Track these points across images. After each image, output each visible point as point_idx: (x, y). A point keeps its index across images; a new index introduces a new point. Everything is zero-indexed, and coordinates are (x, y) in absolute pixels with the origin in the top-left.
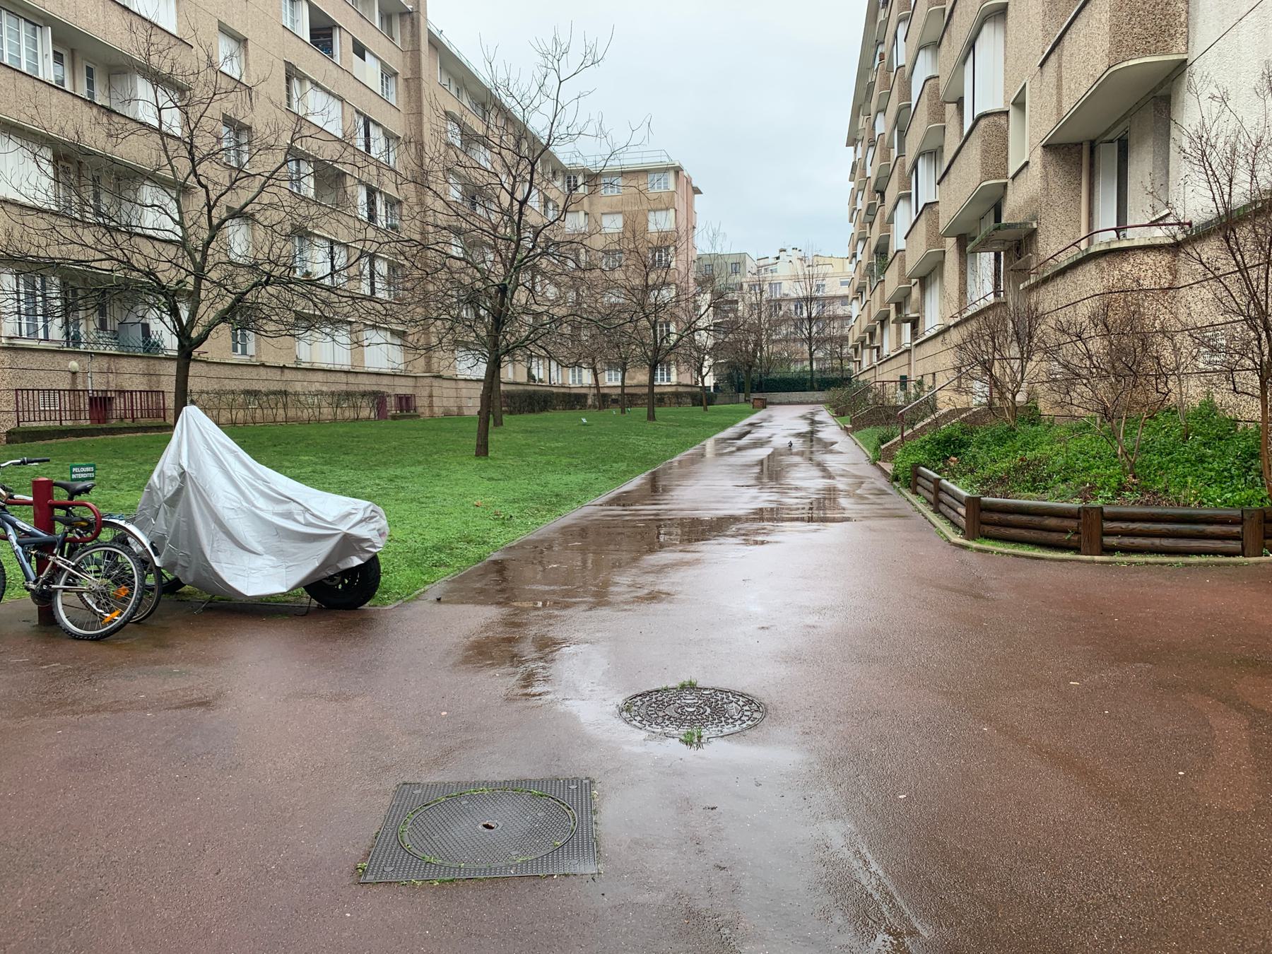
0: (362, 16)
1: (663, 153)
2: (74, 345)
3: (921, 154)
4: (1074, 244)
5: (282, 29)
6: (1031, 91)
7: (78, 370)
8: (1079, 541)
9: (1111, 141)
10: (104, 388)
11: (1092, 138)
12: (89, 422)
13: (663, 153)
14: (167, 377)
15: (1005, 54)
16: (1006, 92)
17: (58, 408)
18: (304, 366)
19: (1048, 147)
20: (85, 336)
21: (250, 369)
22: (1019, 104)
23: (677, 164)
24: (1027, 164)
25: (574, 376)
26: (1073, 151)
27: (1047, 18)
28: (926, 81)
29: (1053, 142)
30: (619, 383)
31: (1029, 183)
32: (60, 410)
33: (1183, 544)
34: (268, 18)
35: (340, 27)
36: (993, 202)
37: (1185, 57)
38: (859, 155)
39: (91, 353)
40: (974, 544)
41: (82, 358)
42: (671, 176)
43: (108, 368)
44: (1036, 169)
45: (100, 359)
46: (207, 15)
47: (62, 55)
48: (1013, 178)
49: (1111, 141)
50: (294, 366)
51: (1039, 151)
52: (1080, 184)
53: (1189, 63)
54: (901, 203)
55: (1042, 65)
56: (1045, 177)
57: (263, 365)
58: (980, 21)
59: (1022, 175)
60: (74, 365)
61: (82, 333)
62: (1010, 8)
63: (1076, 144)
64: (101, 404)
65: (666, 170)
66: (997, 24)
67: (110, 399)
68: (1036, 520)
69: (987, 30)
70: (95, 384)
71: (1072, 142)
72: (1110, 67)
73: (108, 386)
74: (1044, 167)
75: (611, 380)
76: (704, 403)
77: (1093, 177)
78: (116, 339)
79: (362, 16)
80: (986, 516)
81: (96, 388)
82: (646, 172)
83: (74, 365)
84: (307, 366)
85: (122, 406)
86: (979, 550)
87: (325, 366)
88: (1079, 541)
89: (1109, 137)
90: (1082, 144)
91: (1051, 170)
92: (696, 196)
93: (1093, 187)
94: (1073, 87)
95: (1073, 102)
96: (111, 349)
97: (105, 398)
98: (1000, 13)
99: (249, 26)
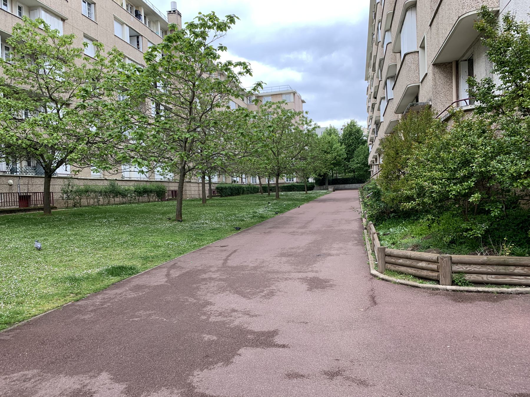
0: (152, 31)
1: (288, 86)
2: (11, 173)
3: (388, 78)
4: (445, 110)
5: (114, 36)
6: (427, 39)
7: (12, 184)
8: (438, 276)
9: (466, 60)
10: (26, 191)
11: (457, 59)
12: (18, 207)
13: (288, 86)
14: (58, 186)
15: (417, 25)
16: (418, 43)
17: (3, 201)
18: (125, 179)
19: (436, 65)
20: (19, 169)
21: (99, 181)
22: (422, 47)
23: (294, 91)
24: (426, 74)
25: (253, 180)
26: (448, 66)
27: (433, 3)
28: (387, 45)
29: (436, 62)
30: (275, 182)
31: (428, 84)
32: (4, 202)
33: (501, 279)
34: (108, 32)
35: (142, 36)
36: (415, 96)
37: (498, 9)
38: (369, 83)
39: (19, 176)
40: (382, 276)
41: (15, 178)
42: (292, 95)
43: (28, 183)
44: (430, 77)
45: (24, 179)
46: (78, 31)
47: (9, 48)
48: (422, 82)
49: (466, 60)
50: (121, 179)
51: (431, 67)
52: (452, 82)
53: (500, 12)
54: (382, 100)
55: (430, 25)
56: (434, 79)
57: (106, 179)
58: (405, 11)
59: (425, 80)
60: (11, 182)
61: (18, 168)
62: (418, 3)
63: (449, 63)
64: (25, 199)
65: (290, 93)
66: (412, 11)
67: (30, 196)
68: (414, 263)
69: (408, 14)
70: (24, 190)
71: (447, 61)
72: (459, 17)
73: (28, 191)
74: (434, 75)
75: (265, 181)
76: (306, 190)
77: (458, 78)
78: (35, 170)
79: (152, 31)
80: (388, 259)
81: (22, 192)
82: (281, 94)
83: (11, 182)
84: (128, 179)
85: (35, 199)
86: (383, 279)
87: (136, 179)
88: (438, 276)
89: (464, 58)
90: (452, 63)
91: (437, 76)
92: (303, 104)
93: (458, 84)
94: (444, 32)
95: (444, 39)
96: (29, 174)
97: (27, 196)
98: (413, 6)
99: (99, 36)
